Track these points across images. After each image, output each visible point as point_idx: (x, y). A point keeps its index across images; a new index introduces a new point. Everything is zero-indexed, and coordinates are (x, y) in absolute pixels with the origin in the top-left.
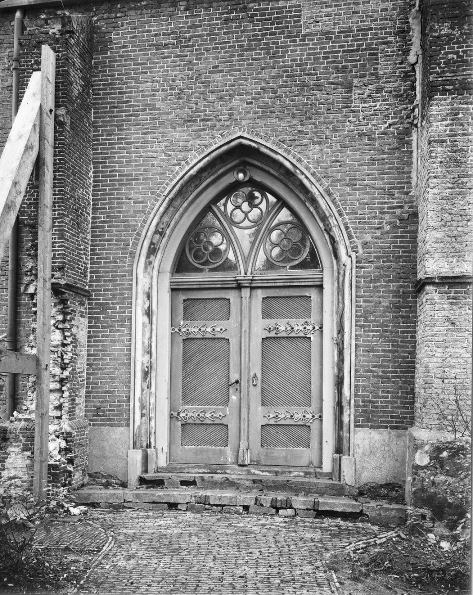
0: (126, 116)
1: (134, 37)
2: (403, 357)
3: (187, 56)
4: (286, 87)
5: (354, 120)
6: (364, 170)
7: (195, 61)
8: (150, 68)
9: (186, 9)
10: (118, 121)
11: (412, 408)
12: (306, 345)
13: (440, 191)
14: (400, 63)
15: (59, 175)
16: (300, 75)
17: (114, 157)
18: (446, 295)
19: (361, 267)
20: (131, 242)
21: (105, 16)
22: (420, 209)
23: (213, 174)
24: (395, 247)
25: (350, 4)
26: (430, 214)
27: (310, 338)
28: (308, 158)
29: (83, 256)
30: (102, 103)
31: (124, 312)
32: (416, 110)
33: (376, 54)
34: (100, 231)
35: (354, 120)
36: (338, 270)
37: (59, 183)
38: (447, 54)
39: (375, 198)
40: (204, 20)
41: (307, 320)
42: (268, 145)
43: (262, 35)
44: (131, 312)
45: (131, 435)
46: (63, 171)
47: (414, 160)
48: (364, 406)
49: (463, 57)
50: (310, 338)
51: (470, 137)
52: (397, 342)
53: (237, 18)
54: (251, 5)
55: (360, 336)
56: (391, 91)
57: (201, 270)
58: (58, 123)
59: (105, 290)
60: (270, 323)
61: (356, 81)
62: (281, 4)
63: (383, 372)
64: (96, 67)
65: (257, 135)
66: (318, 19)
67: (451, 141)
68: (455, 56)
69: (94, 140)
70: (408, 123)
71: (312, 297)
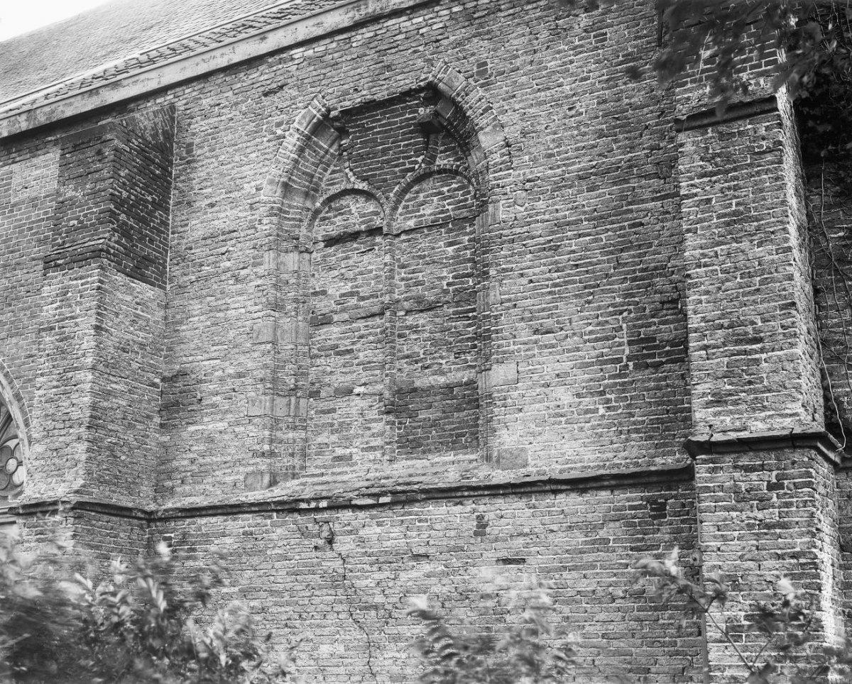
13: (45, 392)
18: (34, 530)
38: (69, 220)
51: (77, 320)
66: (26, 185)
68: (76, 222)
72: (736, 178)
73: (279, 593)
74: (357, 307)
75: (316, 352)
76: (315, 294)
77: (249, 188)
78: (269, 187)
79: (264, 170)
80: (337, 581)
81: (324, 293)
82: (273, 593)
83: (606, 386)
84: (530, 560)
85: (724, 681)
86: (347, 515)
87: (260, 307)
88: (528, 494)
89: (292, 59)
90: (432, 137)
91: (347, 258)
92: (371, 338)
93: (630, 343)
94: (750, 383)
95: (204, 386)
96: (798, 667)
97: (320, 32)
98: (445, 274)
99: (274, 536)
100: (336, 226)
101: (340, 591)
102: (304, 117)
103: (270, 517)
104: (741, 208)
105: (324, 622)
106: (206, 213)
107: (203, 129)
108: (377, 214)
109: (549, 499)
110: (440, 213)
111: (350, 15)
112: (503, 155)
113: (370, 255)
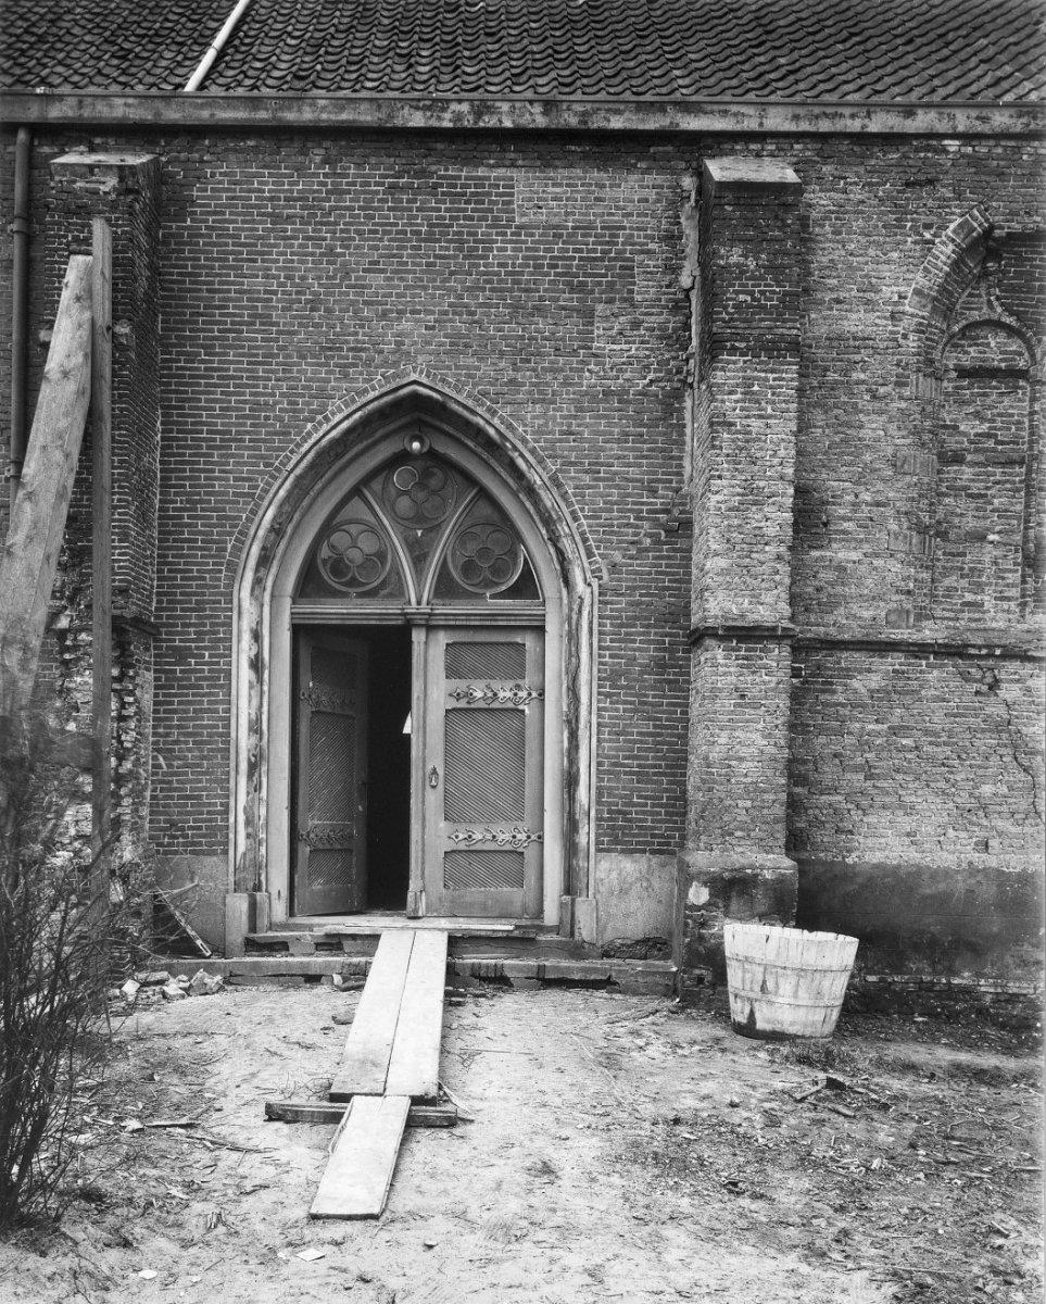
0: (219, 331)
1: (233, 198)
2: (669, 743)
3: (325, 239)
4: (490, 306)
5: (596, 369)
6: (612, 449)
7: (339, 250)
8: (262, 253)
9: (325, 161)
10: (205, 338)
11: (683, 822)
12: (516, 723)
14: (668, 286)
15: (120, 435)
17: (199, 400)
19: (607, 603)
20: (229, 546)
21: (183, 156)
22: (696, 517)
23: (366, 439)
24: (657, 573)
25: (591, 185)
26: (712, 531)
27: (523, 711)
29: (149, 568)
30: (177, 306)
31: (218, 663)
32: (691, 361)
33: (632, 268)
34: (174, 525)
35: (596, 369)
36: (570, 603)
37: (121, 449)
39: (629, 495)
40: (354, 184)
41: (520, 682)
42: (459, 398)
43: (451, 218)
44: (230, 664)
45: (231, 869)
46: (126, 429)
47: (688, 439)
48: (610, 819)
49: (759, 300)
50: (523, 711)
52: (660, 719)
53: (410, 187)
54: (434, 168)
55: (605, 709)
57: (345, 595)
58: (117, 346)
59: (184, 625)
60: (460, 685)
61: (600, 307)
62: (963, 1300)
63: (639, 766)
64: (165, 243)
65: (443, 380)
67: (742, 425)
68: (749, 298)
69: (163, 368)
70: (679, 380)
71: (528, 644)
74: (994, 450)
75: (944, 490)
81: (956, 428)
82: (926, 732)
91: (985, 395)
92: (1008, 486)
96: (64, 847)
100: (971, 356)
101: (1004, 735)
103: (927, 658)
106: (831, 309)
108: (1021, 354)
111: (1024, 120)
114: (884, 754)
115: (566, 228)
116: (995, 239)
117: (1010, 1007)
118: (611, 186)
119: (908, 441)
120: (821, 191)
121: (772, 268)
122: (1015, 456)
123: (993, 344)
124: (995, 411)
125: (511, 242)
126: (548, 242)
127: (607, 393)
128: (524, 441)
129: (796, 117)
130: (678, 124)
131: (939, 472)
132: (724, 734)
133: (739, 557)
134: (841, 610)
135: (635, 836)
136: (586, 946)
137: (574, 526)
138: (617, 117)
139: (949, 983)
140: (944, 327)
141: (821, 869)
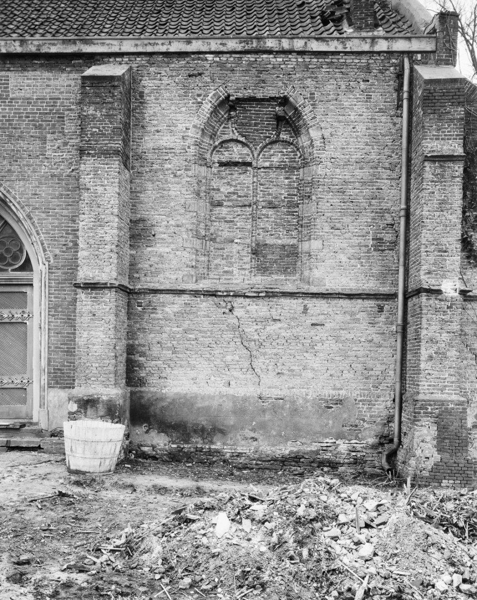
5: (47, 164)
16: (8, 128)
19: (52, 273)
27: (26, 323)
28: (15, 191)
33: (63, 118)
35: (47, 164)
39: (63, 223)
41: (24, 310)
48: (55, 373)
49: (102, 131)
50: (26, 323)
55: (52, 322)
56: (74, 146)
61: (49, 136)
63: (67, 348)
66: (21, 88)
68: (97, 130)
71: (28, 292)
72: (445, 186)
73: (205, 332)
75: (214, 219)
76: (213, 189)
77: (181, 127)
78: (194, 129)
79: (191, 119)
80: (236, 328)
81: (218, 190)
82: (200, 331)
83: (363, 256)
84: (326, 325)
85: (470, 373)
86: (241, 300)
87: (188, 193)
88: (328, 298)
89: (206, 60)
90: (280, 123)
92: (244, 217)
93: (373, 239)
94: (442, 267)
95: (156, 228)
97: (224, 49)
98: (283, 192)
99: (201, 306)
100: (225, 157)
101: (237, 333)
102: (214, 95)
103: (200, 297)
104: (446, 198)
105: (229, 346)
106: (154, 135)
107: (150, 85)
109: (336, 301)
110: (282, 162)
111: (243, 45)
112: (321, 143)
113: (244, 175)
114: (181, 342)
115: (33, 99)
116: (232, 101)
117: (239, 459)
118: (54, 79)
119: (191, 196)
120: (149, 79)
121: (108, 116)
122: (246, 203)
123: (235, 150)
124: (237, 182)
125: (9, 106)
126: (25, 106)
127: (53, 176)
128: (15, 198)
129: (136, 45)
130: (81, 50)
131: (211, 211)
132: (86, 333)
133: (93, 251)
134: (162, 275)
135: (66, 380)
136: (43, 431)
137: (37, 237)
138: (54, 47)
139: (210, 448)
140: (211, 142)
141: (150, 395)
